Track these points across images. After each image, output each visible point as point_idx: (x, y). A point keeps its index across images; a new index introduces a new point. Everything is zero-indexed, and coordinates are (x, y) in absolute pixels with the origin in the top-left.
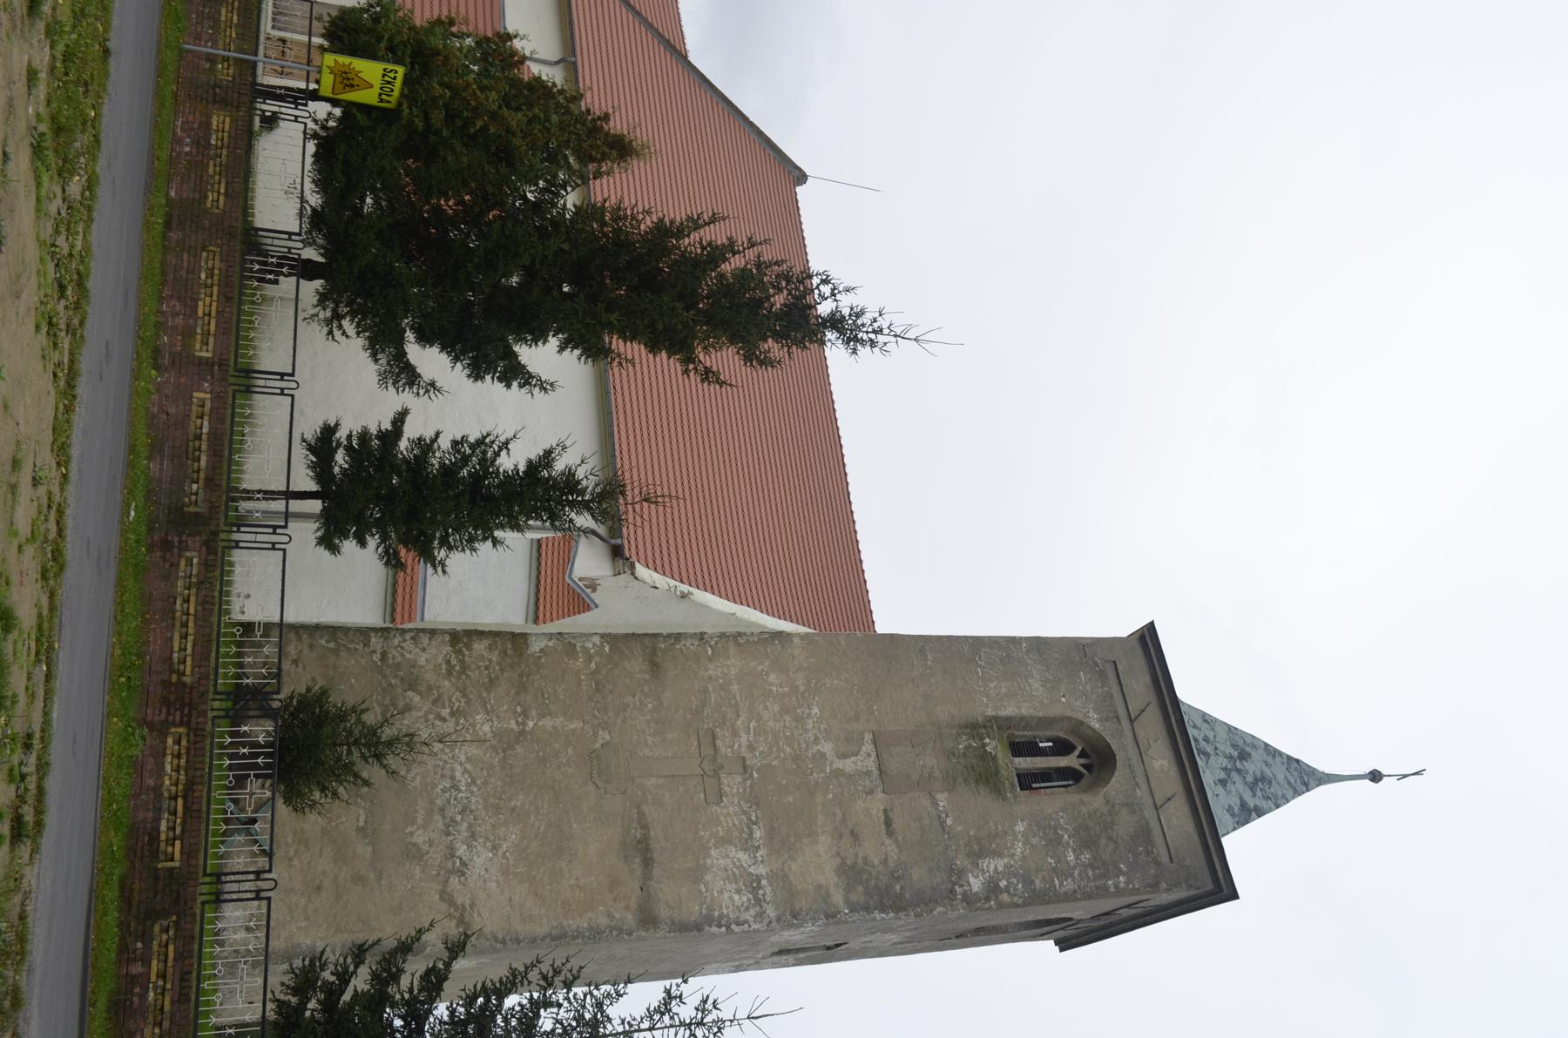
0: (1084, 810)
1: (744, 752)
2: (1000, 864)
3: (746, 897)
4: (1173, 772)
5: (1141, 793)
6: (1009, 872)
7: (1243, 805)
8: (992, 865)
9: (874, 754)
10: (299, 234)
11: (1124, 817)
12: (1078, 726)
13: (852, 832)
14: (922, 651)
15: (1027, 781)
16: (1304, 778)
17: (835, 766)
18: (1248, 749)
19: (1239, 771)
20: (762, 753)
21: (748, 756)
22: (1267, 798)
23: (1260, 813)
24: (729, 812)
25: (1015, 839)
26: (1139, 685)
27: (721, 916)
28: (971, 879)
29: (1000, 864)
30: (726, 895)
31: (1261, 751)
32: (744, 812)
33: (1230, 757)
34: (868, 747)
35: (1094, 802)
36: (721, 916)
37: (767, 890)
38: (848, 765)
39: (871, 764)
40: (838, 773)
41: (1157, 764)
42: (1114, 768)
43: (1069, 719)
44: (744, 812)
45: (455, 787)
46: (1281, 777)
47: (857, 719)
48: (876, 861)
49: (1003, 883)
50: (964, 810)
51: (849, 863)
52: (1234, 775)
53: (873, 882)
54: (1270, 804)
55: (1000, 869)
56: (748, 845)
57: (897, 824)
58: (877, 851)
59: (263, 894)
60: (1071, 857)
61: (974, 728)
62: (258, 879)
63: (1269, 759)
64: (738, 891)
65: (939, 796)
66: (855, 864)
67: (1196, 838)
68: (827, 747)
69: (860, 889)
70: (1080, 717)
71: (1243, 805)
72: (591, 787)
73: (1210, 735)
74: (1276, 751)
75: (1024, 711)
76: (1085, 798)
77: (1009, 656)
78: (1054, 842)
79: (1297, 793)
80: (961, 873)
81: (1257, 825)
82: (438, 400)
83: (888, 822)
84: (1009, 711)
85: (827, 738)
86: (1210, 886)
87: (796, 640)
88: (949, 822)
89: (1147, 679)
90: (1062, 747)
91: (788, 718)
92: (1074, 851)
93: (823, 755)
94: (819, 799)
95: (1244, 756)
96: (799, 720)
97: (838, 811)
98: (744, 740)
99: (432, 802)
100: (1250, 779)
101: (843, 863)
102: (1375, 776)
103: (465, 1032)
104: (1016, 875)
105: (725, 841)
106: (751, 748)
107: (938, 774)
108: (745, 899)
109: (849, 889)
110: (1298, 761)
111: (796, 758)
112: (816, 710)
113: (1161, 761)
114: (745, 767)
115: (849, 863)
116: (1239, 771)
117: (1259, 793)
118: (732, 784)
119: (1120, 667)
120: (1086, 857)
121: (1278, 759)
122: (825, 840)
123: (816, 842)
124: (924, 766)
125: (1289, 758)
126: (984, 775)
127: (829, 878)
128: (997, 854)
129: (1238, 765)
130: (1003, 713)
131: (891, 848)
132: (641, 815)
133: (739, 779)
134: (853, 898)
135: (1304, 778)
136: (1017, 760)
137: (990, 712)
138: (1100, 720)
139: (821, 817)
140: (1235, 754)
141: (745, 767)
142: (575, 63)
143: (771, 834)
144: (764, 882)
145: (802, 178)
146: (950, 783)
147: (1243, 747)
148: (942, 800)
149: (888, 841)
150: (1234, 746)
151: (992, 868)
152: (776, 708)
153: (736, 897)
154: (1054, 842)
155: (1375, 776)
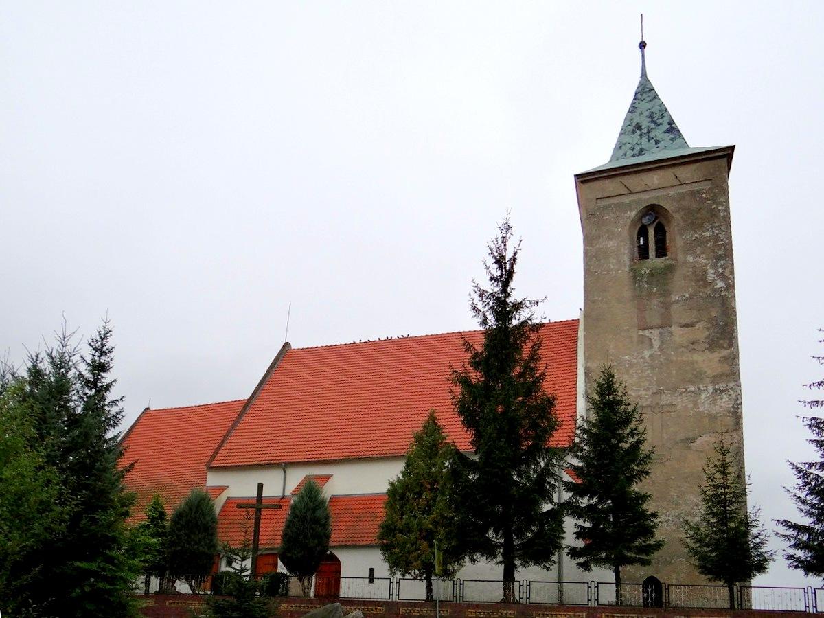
0: (682, 224)
1: (649, 393)
2: (710, 271)
3: (725, 396)
4: (661, 173)
5: (672, 192)
6: (715, 266)
7: (668, 131)
8: (711, 276)
9: (650, 330)
10: (742, 609)
11: (686, 203)
12: (634, 223)
13: (692, 344)
14: (593, 302)
15: (662, 251)
16: (645, 91)
17: (657, 349)
18: (634, 124)
19: (649, 132)
20: (650, 385)
21: (651, 391)
22: (662, 116)
23: (671, 122)
24: (681, 401)
25: (697, 262)
26: (611, 186)
27: (733, 407)
28: (718, 286)
29: (710, 271)
30: (723, 404)
31: (634, 116)
32: (681, 394)
33: (641, 135)
34: (647, 333)
35: (677, 217)
36: (733, 407)
37: (721, 386)
38: (656, 344)
39: (656, 332)
40: (661, 349)
41: (656, 182)
42: (658, 205)
43: (630, 227)
44: (681, 394)
45: (667, 521)
46: (648, 106)
47: (631, 337)
48: (707, 333)
49: (721, 270)
50: (681, 288)
51: (708, 346)
52: (652, 134)
53: (718, 335)
54: (665, 114)
55: (713, 271)
56: (699, 392)
57: (687, 321)
58: (701, 332)
59: (528, 584)
60: (707, 234)
61: (635, 276)
62: (813, 607)
63: (638, 111)
64: (721, 399)
65: (673, 300)
66: (708, 343)
67: (698, 164)
68: (647, 354)
69: (721, 341)
70: (629, 221)
71: (668, 131)
72: (667, 463)
73: (630, 146)
74: (632, 106)
75: (626, 252)
76: (674, 223)
77: (595, 257)
78: (700, 242)
79: (656, 97)
80: (714, 290)
81: (679, 124)
82: (665, 547)
83: (687, 326)
84: (626, 259)
85: (642, 353)
86: (726, 159)
87: (589, 365)
88: (687, 295)
89: (607, 181)
90: (643, 232)
91: (631, 371)
92: (704, 232)
93: (651, 356)
94: (674, 358)
95: (638, 127)
96: (632, 365)
97: (681, 350)
98: (644, 393)
99: (674, 531)
100: (652, 125)
101: (708, 349)
102: (643, 45)
103: (5, 431)
104: (716, 263)
105: (696, 405)
106: (647, 389)
107: (661, 299)
108: (725, 396)
109: (722, 347)
110: (636, 94)
111: (653, 368)
112: (627, 357)
113: (655, 179)
114: (657, 393)
115: (708, 346)
116: (649, 132)
117: (660, 121)
118: (666, 399)
119: (600, 196)
120: (707, 226)
121: (636, 105)
122: (696, 357)
123: (697, 362)
124: (657, 306)
125: (635, 99)
126: (662, 277)
127: (716, 356)
128: (705, 272)
129: (645, 131)
130: (628, 263)
131: (700, 325)
132: (682, 441)
133: (663, 396)
134: (726, 345)
135: (645, 91)
136: (650, 257)
137: (627, 269)
138: (631, 211)
139: (684, 359)
140: (638, 132)
141: (657, 393)
142: (285, 463)
143: (692, 382)
144: (717, 387)
145: (287, 345)
146: (666, 293)
147: (633, 127)
148: (675, 297)
149: (697, 326)
150: (634, 132)
151: (713, 276)
152: (626, 376)
153: (724, 400)
154: (700, 242)
155: (643, 45)
